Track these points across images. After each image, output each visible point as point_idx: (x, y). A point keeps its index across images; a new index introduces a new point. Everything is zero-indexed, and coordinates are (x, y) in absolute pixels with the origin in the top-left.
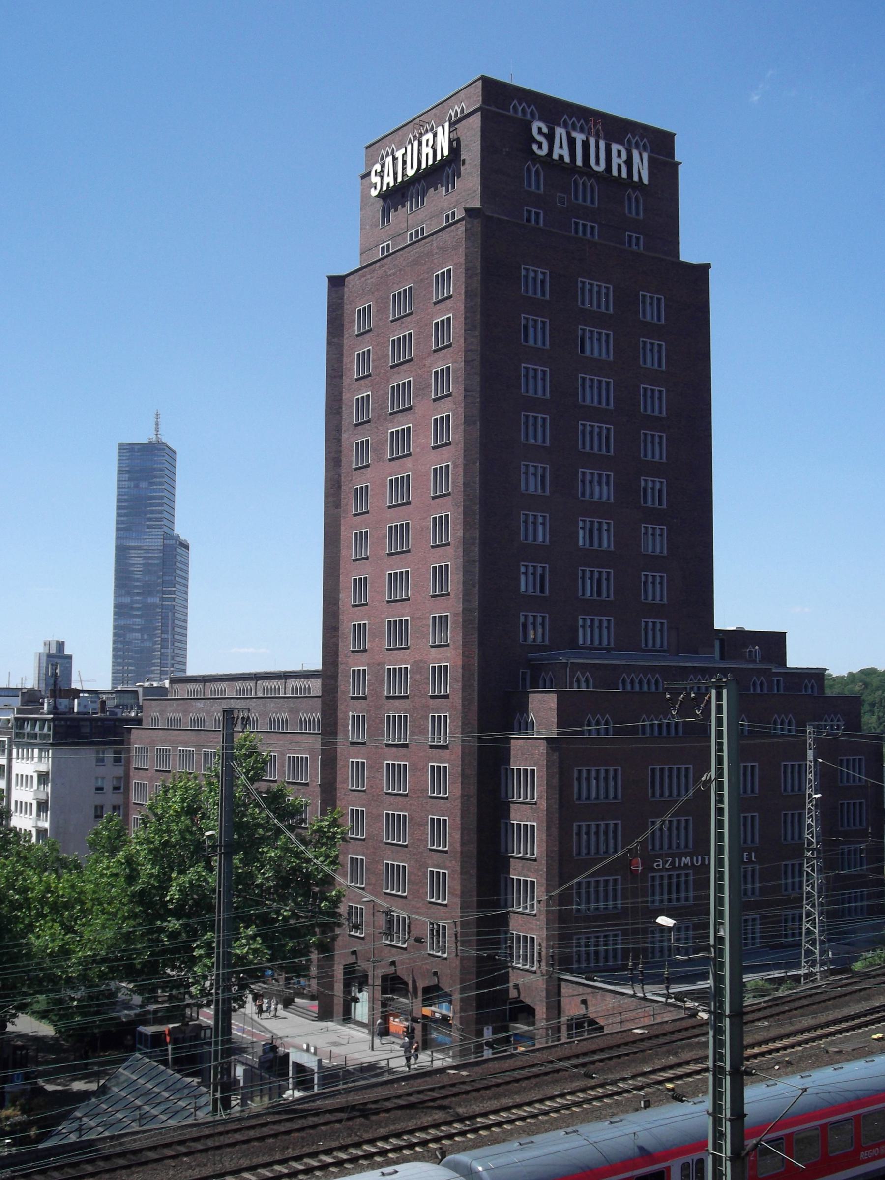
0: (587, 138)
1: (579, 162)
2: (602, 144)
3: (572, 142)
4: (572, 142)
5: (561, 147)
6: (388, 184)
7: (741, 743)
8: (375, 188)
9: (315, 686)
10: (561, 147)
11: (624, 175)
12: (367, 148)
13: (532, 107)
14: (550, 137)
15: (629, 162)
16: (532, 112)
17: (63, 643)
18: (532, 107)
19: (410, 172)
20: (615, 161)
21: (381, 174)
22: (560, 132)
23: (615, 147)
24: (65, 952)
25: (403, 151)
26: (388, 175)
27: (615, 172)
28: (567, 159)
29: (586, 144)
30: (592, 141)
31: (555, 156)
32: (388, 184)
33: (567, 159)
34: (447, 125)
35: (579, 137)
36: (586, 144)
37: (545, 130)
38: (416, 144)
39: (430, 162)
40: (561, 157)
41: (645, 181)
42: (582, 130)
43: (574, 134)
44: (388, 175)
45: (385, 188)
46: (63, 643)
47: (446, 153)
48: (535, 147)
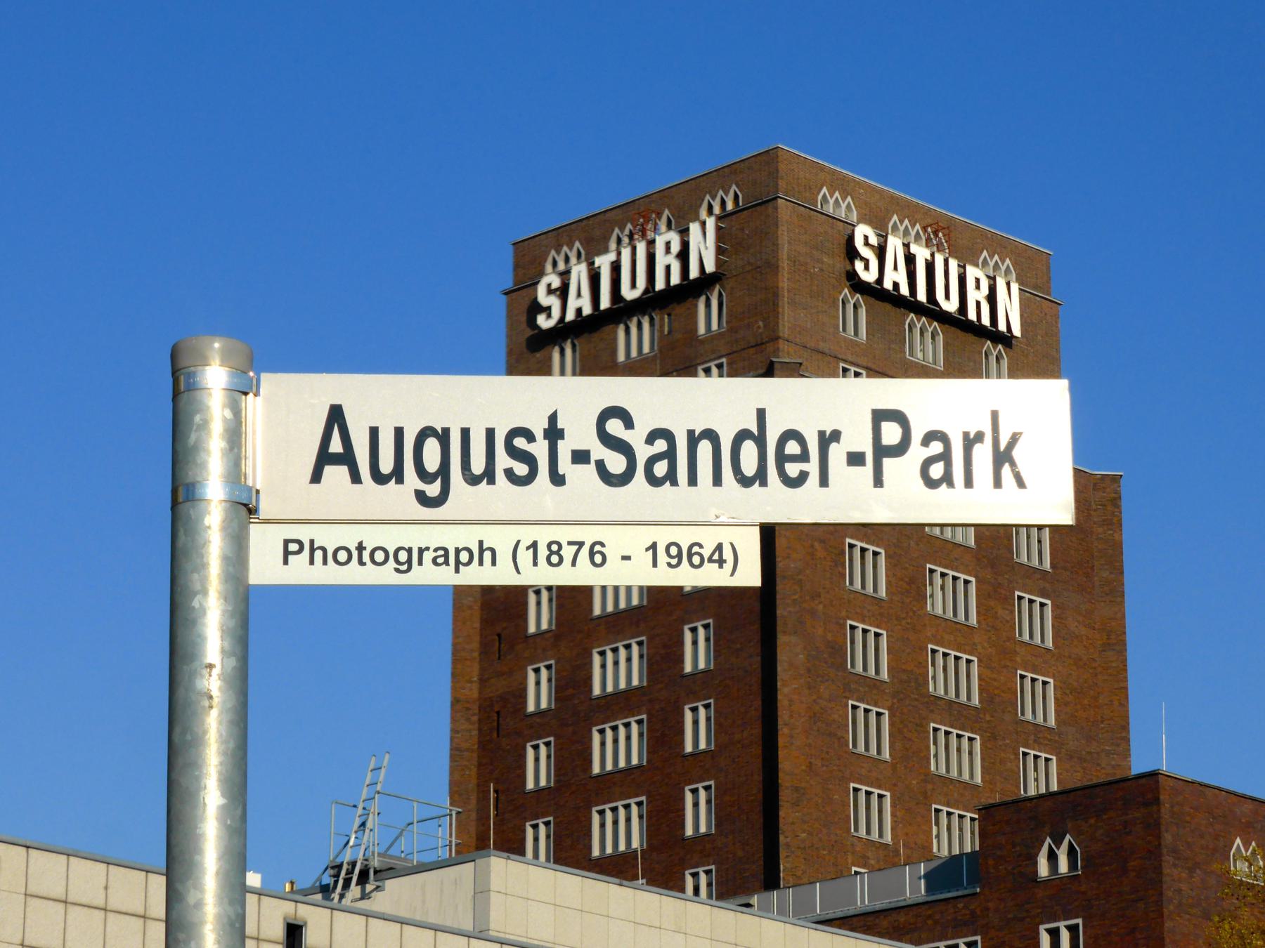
0: (932, 255)
1: (922, 296)
2: (953, 264)
3: (910, 260)
4: (910, 260)
5: (579, 295)
6: (579, 311)
7: (964, 857)
8: (549, 316)
9: (964, 528)
10: (579, 295)
11: (986, 321)
12: (514, 244)
13: (849, 199)
14: (881, 252)
15: (992, 298)
16: (849, 206)
17: (875, 486)
18: (849, 199)
19: (660, 285)
20: (973, 296)
21: (563, 292)
22: (894, 244)
23: (972, 272)
24: (843, 833)
25: (612, 257)
26: (896, 268)
27: (972, 315)
28: (904, 290)
29: (930, 267)
30: (939, 260)
31: (888, 285)
32: (579, 311)
33: (904, 290)
34: (711, 223)
35: (921, 254)
36: (930, 267)
37: (874, 240)
38: (641, 248)
39: (675, 279)
40: (896, 285)
41: (1017, 331)
42: (928, 244)
43: (914, 249)
44: (896, 268)
45: (570, 316)
46: (875, 486)
47: (710, 267)
48: (859, 266)
